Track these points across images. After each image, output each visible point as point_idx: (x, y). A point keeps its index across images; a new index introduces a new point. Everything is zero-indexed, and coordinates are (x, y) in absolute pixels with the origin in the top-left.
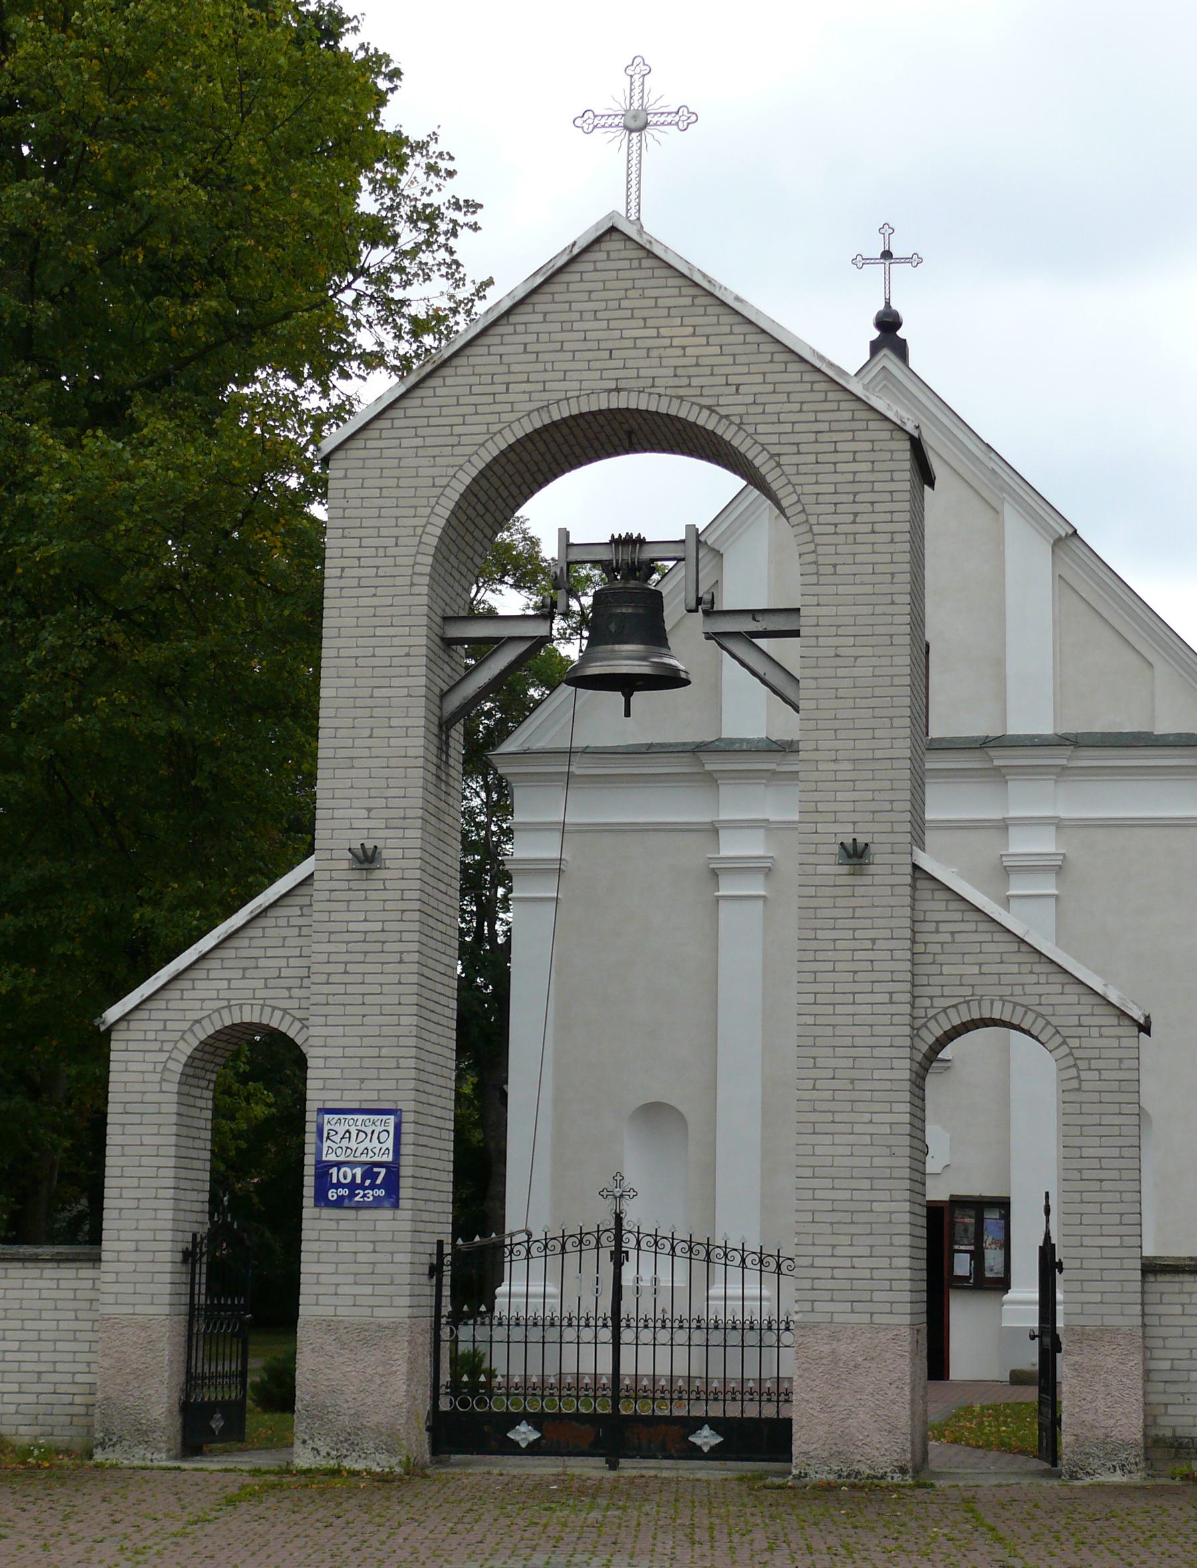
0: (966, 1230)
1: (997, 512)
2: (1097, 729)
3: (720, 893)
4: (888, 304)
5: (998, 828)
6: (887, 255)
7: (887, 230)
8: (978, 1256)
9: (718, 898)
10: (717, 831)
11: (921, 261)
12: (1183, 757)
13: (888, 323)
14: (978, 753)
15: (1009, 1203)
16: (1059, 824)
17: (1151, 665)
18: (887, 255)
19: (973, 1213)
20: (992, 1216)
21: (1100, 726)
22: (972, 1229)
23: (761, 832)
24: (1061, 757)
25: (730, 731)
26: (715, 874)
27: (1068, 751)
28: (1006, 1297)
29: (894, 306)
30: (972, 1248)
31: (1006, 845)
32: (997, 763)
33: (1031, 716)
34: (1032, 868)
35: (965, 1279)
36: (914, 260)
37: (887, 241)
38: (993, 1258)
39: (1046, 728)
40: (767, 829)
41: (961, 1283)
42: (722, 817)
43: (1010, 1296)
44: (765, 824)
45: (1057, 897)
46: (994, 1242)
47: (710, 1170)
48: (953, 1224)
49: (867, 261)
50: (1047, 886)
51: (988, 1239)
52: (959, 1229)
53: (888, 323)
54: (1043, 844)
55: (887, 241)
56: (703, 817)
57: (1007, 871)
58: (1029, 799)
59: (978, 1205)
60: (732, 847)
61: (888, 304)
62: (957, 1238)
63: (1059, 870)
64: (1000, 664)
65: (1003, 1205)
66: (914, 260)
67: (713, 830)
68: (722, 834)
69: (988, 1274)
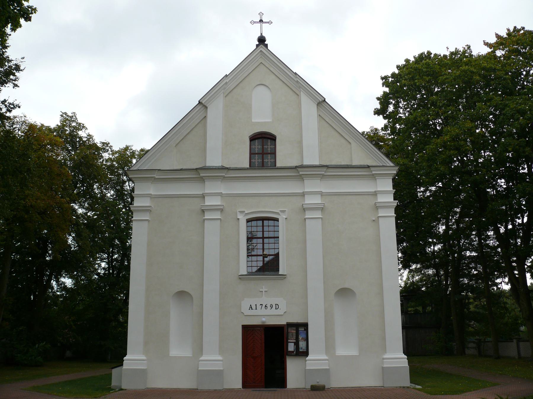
0: (292, 335)
1: (298, 95)
2: (333, 164)
3: (205, 218)
4: (261, 34)
5: (302, 196)
6: (261, 21)
7: (261, 14)
8: (297, 344)
9: (204, 220)
10: (204, 197)
11: (272, 23)
12: (364, 172)
13: (262, 40)
14: (367, 169)
15: (307, 325)
16: (322, 194)
17: (350, 143)
18: (261, 21)
19: (295, 328)
20: (301, 329)
21: (334, 163)
22: (295, 334)
23: (220, 197)
24: (322, 172)
25: (209, 164)
26: (203, 211)
27: (325, 169)
28: (307, 358)
29: (263, 35)
30: (295, 341)
31: (377, 199)
32: (374, 172)
33: (311, 158)
34: (213, 209)
35: (293, 352)
36: (270, 23)
37: (261, 17)
38: (302, 344)
39: (317, 163)
40: (151, 198)
41: (291, 354)
42: (206, 192)
43: (309, 358)
44: (220, 194)
45: (322, 218)
46: (302, 339)
47: (201, 315)
48: (288, 332)
49: (255, 22)
50: (318, 214)
51: (300, 338)
52: (290, 335)
53: (262, 40)
54: (316, 200)
55: (261, 17)
56: (301, 191)
57: (304, 210)
58: (312, 185)
59: (297, 326)
60: (209, 202)
61: (261, 34)
62: (289, 338)
63: (322, 209)
64: (300, 143)
65: (305, 326)
66: (270, 23)
67: (203, 196)
68: (378, 195)
69: (300, 350)
